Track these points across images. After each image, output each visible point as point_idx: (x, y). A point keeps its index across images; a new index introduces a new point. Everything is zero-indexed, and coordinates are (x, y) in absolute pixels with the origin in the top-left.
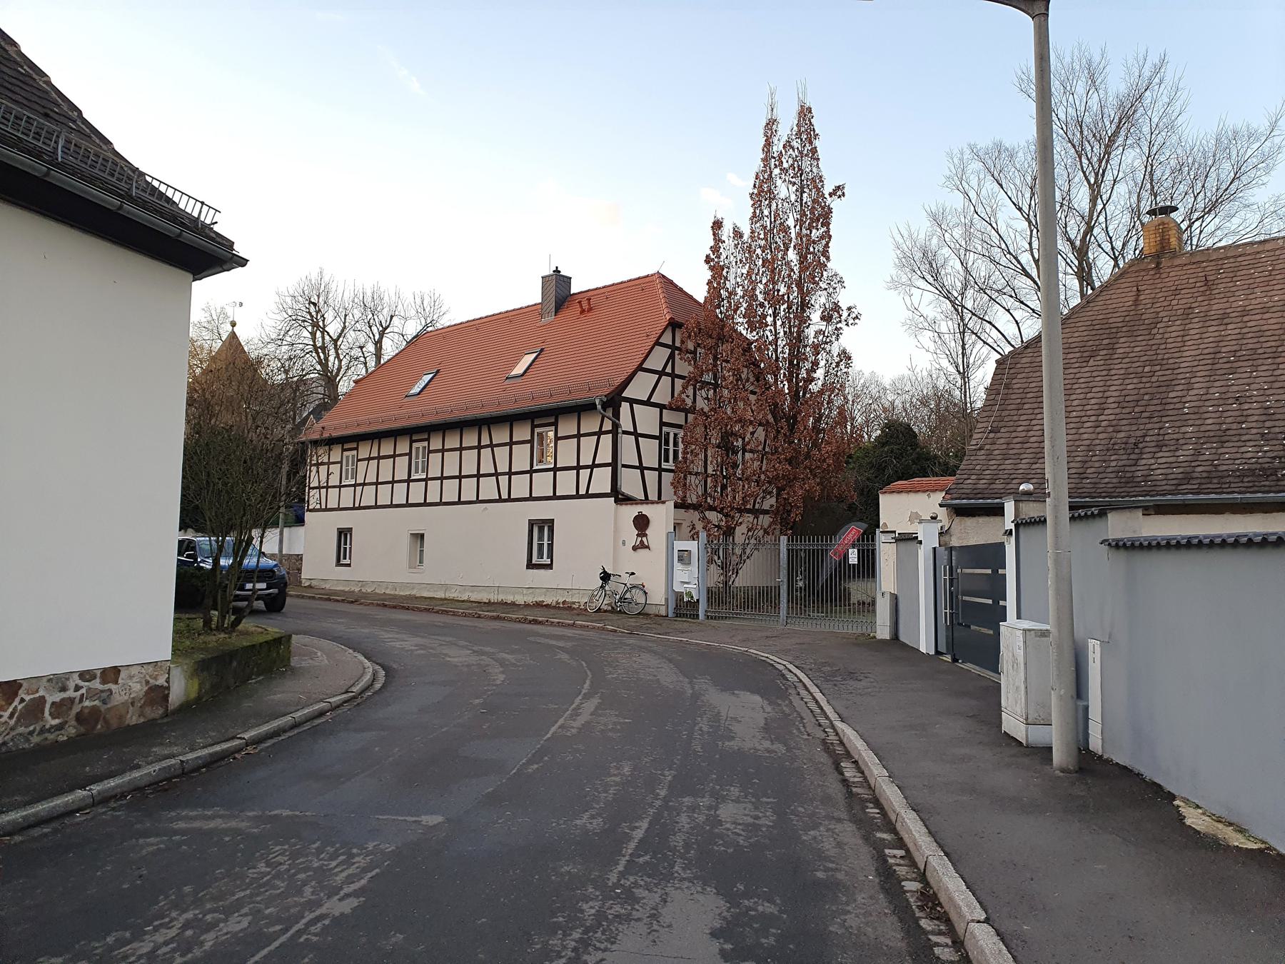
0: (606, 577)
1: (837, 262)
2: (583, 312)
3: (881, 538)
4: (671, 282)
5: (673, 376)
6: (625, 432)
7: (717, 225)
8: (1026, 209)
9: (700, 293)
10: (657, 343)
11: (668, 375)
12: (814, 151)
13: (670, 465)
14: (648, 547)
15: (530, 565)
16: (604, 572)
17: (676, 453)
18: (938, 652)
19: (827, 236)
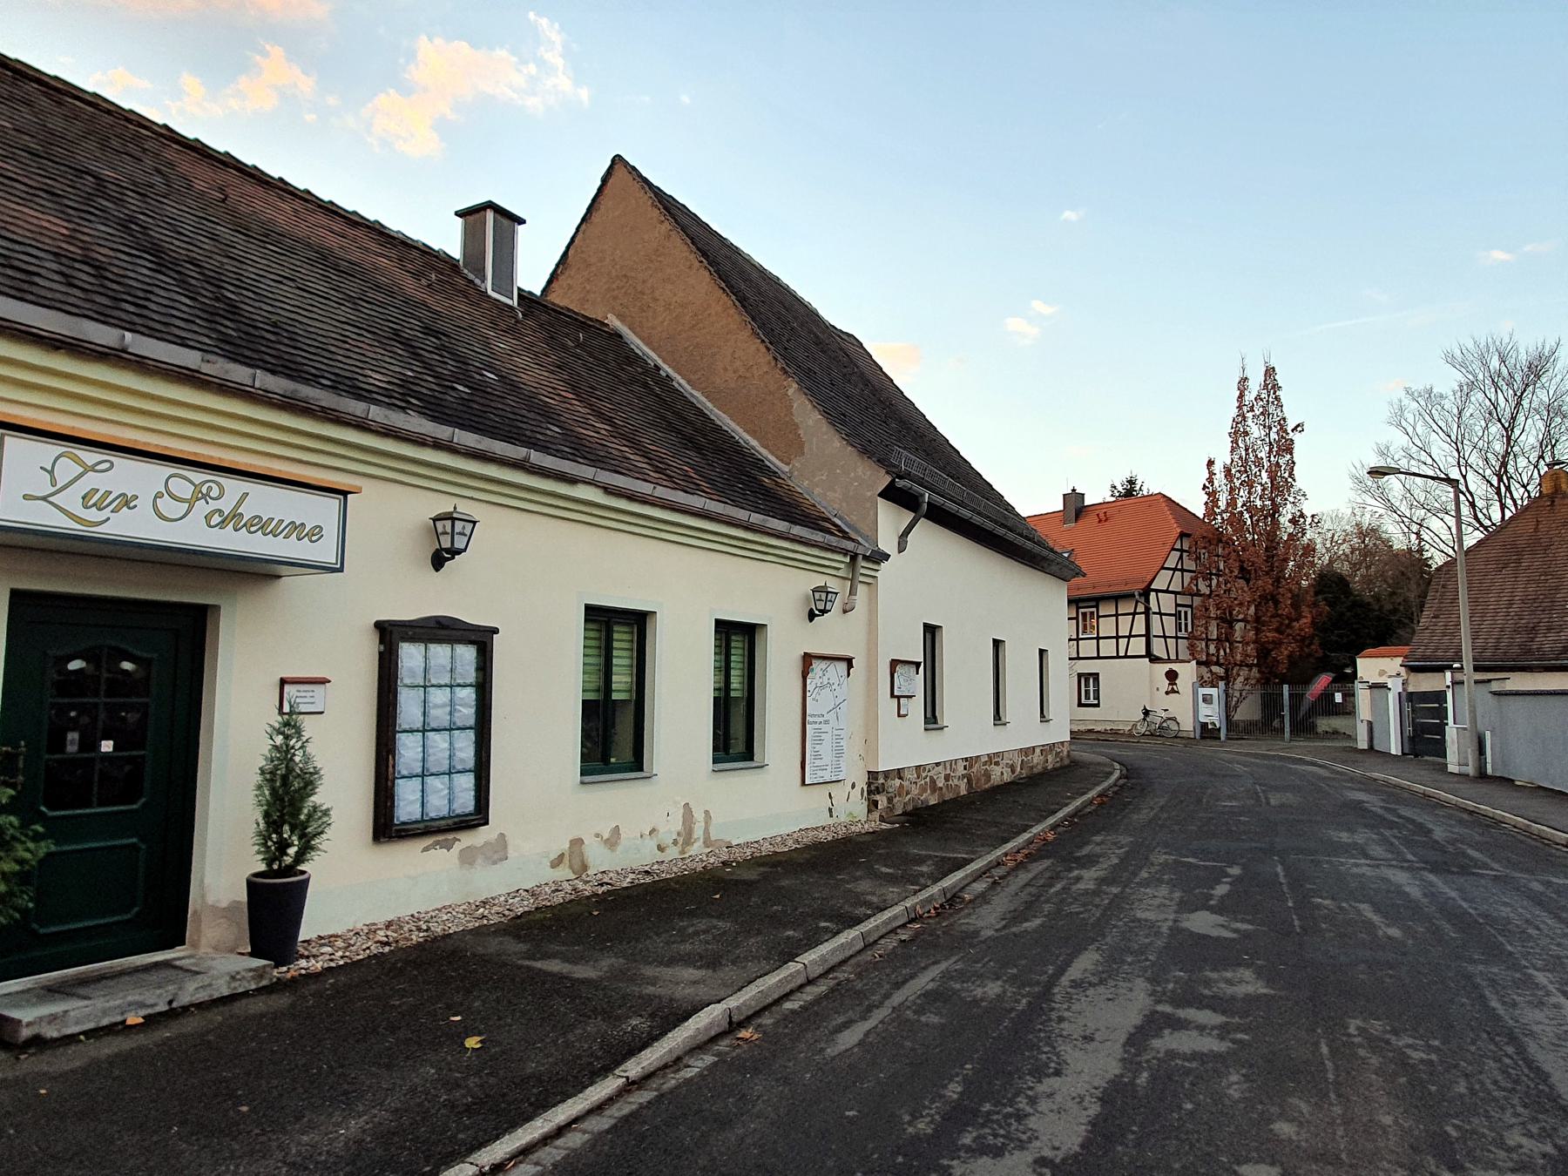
0: (1146, 713)
1: (1302, 478)
2: (1100, 521)
3: (1357, 685)
4: (1170, 499)
5: (1182, 570)
6: (1154, 613)
7: (1210, 463)
8: (1454, 438)
9: (1200, 511)
10: (1173, 549)
11: (1179, 570)
12: (1277, 398)
13: (1182, 634)
14: (1178, 692)
15: (1080, 705)
16: (1145, 708)
17: (1186, 625)
18: (1403, 754)
19: (1292, 464)
